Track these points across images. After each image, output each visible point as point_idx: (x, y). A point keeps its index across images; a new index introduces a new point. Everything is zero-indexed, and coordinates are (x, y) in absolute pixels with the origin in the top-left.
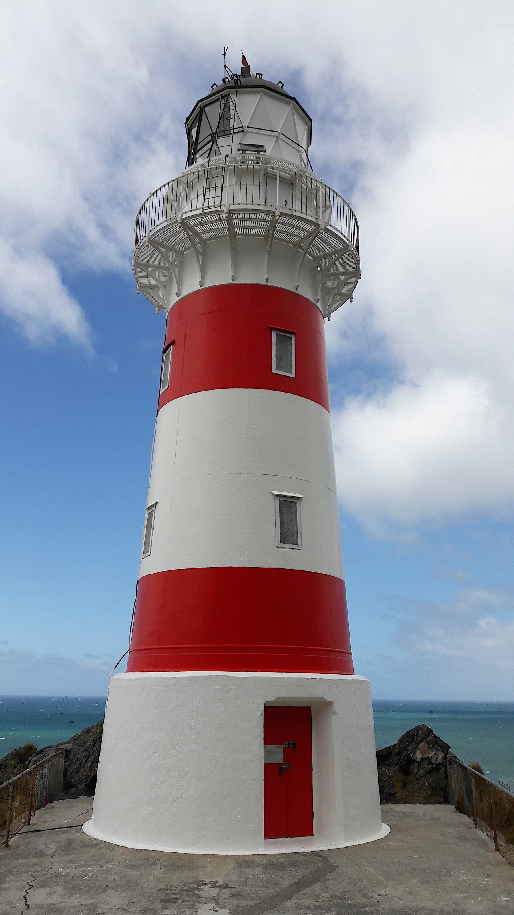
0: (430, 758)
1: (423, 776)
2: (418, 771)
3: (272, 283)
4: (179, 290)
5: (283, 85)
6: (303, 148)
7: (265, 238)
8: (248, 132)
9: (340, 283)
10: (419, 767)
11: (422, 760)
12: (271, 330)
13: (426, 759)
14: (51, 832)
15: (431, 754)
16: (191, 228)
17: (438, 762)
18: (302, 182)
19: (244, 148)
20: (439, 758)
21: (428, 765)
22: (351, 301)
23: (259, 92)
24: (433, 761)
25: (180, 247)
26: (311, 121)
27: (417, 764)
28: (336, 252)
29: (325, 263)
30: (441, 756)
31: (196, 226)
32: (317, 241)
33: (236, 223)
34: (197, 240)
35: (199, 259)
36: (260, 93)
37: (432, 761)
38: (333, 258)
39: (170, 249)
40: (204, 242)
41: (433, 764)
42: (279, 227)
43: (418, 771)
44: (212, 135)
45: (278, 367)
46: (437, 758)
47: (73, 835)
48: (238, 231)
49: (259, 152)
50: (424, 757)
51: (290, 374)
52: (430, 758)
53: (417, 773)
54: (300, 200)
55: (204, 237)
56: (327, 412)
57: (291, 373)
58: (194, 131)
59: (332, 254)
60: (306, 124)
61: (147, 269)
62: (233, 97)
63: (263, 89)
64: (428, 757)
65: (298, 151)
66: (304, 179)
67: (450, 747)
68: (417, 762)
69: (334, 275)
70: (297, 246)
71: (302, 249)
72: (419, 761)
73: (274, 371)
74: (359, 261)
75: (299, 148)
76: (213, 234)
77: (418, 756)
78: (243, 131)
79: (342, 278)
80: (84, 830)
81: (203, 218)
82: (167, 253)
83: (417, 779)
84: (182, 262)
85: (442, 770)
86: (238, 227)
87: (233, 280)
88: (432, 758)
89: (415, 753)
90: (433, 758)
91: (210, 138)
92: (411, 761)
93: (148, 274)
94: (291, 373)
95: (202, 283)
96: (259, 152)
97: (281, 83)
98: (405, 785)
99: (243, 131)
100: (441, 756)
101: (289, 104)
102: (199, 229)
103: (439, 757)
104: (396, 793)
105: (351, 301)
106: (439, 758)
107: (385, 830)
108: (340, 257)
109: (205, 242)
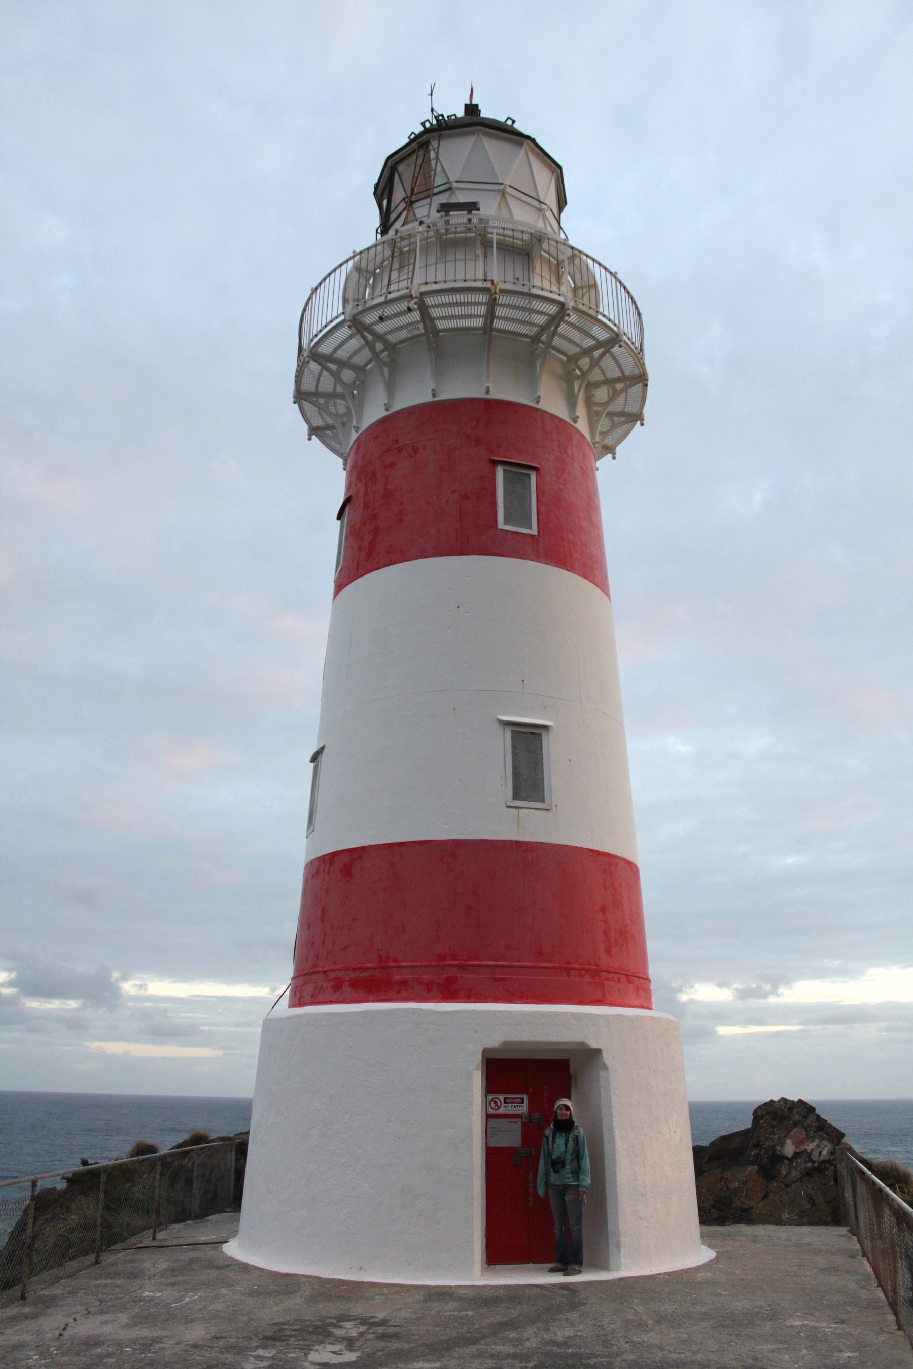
0: (809, 1151)
1: (797, 1181)
2: (789, 1173)
3: (495, 395)
4: (358, 422)
5: (514, 122)
6: (546, 205)
7: (484, 332)
8: (458, 188)
9: (615, 395)
10: (790, 1167)
11: (796, 1155)
12: (494, 463)
13: (802, 1153)
14: (174, 1249)
15: (810, 1147)
16: (368, 328)
17: (822, 1158)
18: (541, 249)
19: (446, 208)
20: (825, 1152)
21: (806, 1162)
22: (642, 425)
23: (473, 133)
24: (815, 1157)
25: (359, 360)
26: (560, 167)
27: (786, 1162)
28: (600, 344)
29: (585, 362)
30: (827, 1149)
31: (374, 323)
32: (563, 328)
33: (434, 313)
34: (379, 346)
35: (383, 372)
36: (474, 134)
37: (813, 1157)
38: (597, 354)
39: (343, 364)
40: (391, 347)
41: (813, 1162)
42: (499, 311)
43: (789, 1173)
44: (406, 200)
45: (506, 521)
46: (821, 1152)
47: (207, 1253)
48: (441, 325)
49: (469, 212)
50: (798, 1150)
51: (529, 530)
52: (809, 1151)
53: (786, 1176)
54: (547, 280)
55: (392, 338)
56: (605, 596)
57: (531, 529)
58: (385, 202)
59: (618, 380)
60: (553, 173)
61: (317, 400)
62: (434, 144)
63: (479, 128)
64: (806, 1150)
65: (540, 210)
66: (545, 246)
67: (843, 1135)
68: (787, 1158)
69: (606, 382)
70: (535, 339)
71: (543, 343)
72: (790, 1156)
73: (501, 525)
74: (644, 364)
75: (541, 206)
76: (404, 334)
77: (789, 1149)
78: (450, 189)
79: (619, 386)
80: (224, 1249)
81: (386, 308)
82: (339, 371)
83: (787, 1186)
84: (363, 382)
85: (830, 1172)
86: (440, 318)
87: (434, 396)
88: (811, 1152)
89: (782, 1145)
90: (814, 1152)
91: (403, 205)
92: (777, 1158)
93: (320, 408)
94: (531, 529)
95: (389, 407)
96: (469, 212)
97: (511, 119)
98: (766, 1196)
99: (450, 189)
100: (827, 1149)
101: (521, 144)
102: (381, 328)
103: (822, 1149)
104: (751, 1208)
105: (642, 425)
106: (825, 1152)
107: (707, 1255)
108: (608, 351)
109: (438, 334)
